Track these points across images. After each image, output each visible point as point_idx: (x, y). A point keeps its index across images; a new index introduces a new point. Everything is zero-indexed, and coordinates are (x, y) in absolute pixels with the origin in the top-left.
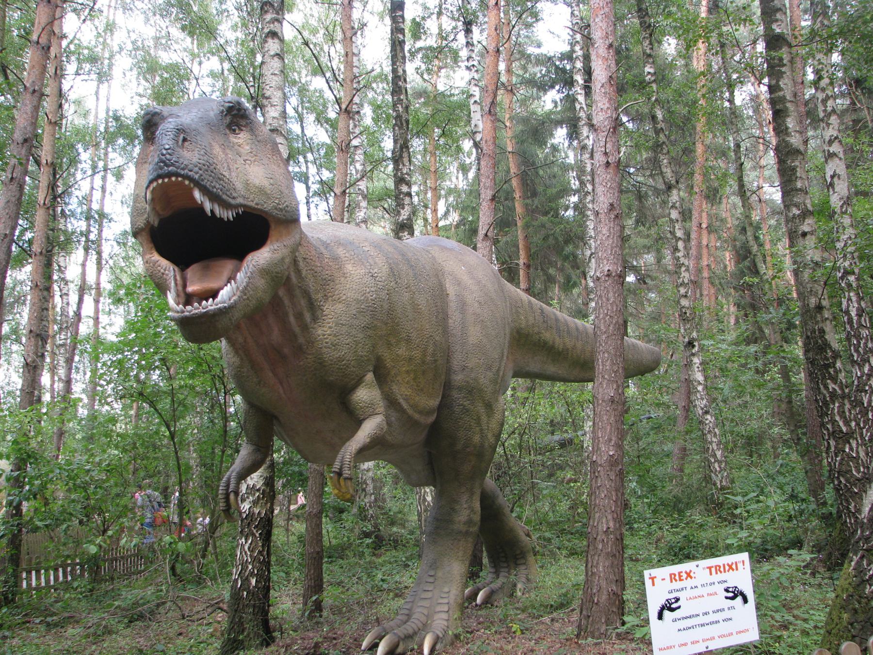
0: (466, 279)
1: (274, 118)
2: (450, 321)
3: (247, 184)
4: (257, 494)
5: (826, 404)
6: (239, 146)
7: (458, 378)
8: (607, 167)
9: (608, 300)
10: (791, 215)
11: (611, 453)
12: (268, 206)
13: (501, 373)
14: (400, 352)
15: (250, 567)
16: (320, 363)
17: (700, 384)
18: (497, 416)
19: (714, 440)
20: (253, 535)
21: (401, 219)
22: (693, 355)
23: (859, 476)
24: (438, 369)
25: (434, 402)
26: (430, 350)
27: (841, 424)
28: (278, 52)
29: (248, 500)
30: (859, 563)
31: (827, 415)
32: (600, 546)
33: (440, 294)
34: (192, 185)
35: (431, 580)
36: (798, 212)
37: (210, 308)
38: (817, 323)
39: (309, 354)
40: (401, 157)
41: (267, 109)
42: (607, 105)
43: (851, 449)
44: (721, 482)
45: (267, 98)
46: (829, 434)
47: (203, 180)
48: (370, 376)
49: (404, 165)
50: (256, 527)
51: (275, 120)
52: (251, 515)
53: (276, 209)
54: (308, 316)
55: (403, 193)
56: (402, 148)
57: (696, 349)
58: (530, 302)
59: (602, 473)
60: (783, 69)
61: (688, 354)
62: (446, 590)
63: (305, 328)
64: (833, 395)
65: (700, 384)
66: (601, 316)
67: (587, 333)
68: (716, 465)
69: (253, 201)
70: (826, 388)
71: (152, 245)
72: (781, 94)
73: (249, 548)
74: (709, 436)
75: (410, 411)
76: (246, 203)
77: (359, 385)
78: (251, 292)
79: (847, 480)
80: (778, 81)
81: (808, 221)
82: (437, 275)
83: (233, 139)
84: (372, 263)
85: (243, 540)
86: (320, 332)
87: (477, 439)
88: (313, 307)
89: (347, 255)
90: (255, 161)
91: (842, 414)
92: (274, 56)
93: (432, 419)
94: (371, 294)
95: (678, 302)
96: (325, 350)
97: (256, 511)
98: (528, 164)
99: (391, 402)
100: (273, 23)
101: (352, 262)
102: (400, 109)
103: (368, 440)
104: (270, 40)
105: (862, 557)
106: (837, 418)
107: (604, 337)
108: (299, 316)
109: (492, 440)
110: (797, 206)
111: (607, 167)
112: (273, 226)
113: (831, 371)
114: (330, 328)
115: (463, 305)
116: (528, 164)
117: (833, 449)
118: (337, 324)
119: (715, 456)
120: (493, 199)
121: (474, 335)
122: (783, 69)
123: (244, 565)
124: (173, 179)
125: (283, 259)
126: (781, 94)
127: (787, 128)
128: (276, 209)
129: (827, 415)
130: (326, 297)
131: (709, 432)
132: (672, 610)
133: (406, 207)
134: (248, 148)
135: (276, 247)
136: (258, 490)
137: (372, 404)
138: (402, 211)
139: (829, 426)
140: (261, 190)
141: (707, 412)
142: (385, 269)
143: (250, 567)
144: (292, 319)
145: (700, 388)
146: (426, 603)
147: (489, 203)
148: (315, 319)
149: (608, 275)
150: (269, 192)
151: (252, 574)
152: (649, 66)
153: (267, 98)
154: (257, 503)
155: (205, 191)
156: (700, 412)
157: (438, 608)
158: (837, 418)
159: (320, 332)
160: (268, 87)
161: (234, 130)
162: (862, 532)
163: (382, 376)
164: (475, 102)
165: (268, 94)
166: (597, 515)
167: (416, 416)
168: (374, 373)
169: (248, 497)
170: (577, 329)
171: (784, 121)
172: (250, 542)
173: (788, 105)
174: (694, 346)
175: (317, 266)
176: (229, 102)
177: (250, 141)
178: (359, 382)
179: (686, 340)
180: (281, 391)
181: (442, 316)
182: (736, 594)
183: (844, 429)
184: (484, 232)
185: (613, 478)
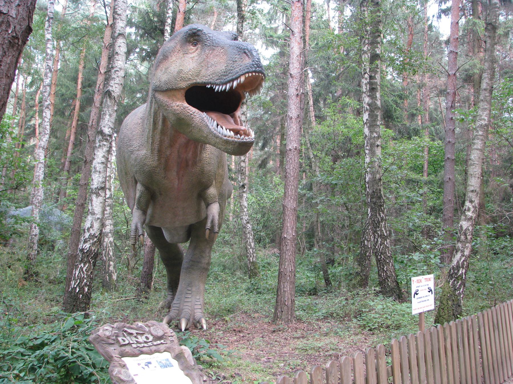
1: (122, 27)
4: (96, 239)
5: (379, 222)
9: (295, 161)
10: (373, 136)
15: (85, 281)
16: (202, 172)
17: (245, 207)
19: (251, 237)
22: (244, 192)
23: (389, 255)
27: (384, 232)
29: (89, 242)
30: (453, 283)
31: (379, 227)
32: (288, 278)
35: (189, 292)
36: (376, 136)
38: (378, 186)
41: (117, 21)
42: (298, 66)
43: (387, 243)
44: (253, 259)
45: (119, 15)
46: (378, 236)
50: (92, 257)
51: (122, 29)
57: (246, 189)
59: (289, 244)
60: (378, 70)
61: (241, 191)
62: (198, 297)
63: (201, 153)
64: (382, 219)
65: (245, 207)
68: (251, 250)
70: (380, 215)
71: (184, 98)
72: (376, 81)
73: (86, 270)
74: (248, 235)
79: (384, 257)
80: (375, 75)
81: (379, 140)
86: (205, 156)
91: (385, 227)
95: (240, 164)
97: (93, 249)
105: (454, 281)
106: (383, 229)
107: (292, 178)
110: (376, 133)
113: (382, 208)
117: (379, 242)
119: (250, 245)
122: (378, 70)
123: (81, 279)
126: (376, 81)
127: (376, 97)
129: (379, 227)
131: (249, 233)
132: (417, 294)
136: (96, 237)
137: (215, 197)
139: (379, 232)
141: (248, 223)
143: (85, 281)
145: (245, 210)
146: (189, 304)
149: (295, 149)
151: (86, 285)
153: (119, 15)
154: (94, 244)
156: (245, 222)
157: (196, 307)
158: (383, 229)
159: (205, 156)
160: (120, 9)
162: (453, 271)
165: (119, 12)
166: (287, 263)
169: (89, 241)
171: (376, 93)
172: (87, 266)
173: (378, 87)
174: (245, 188)
179: (241, 184)
182: (430, 291)
183: (385, 234)
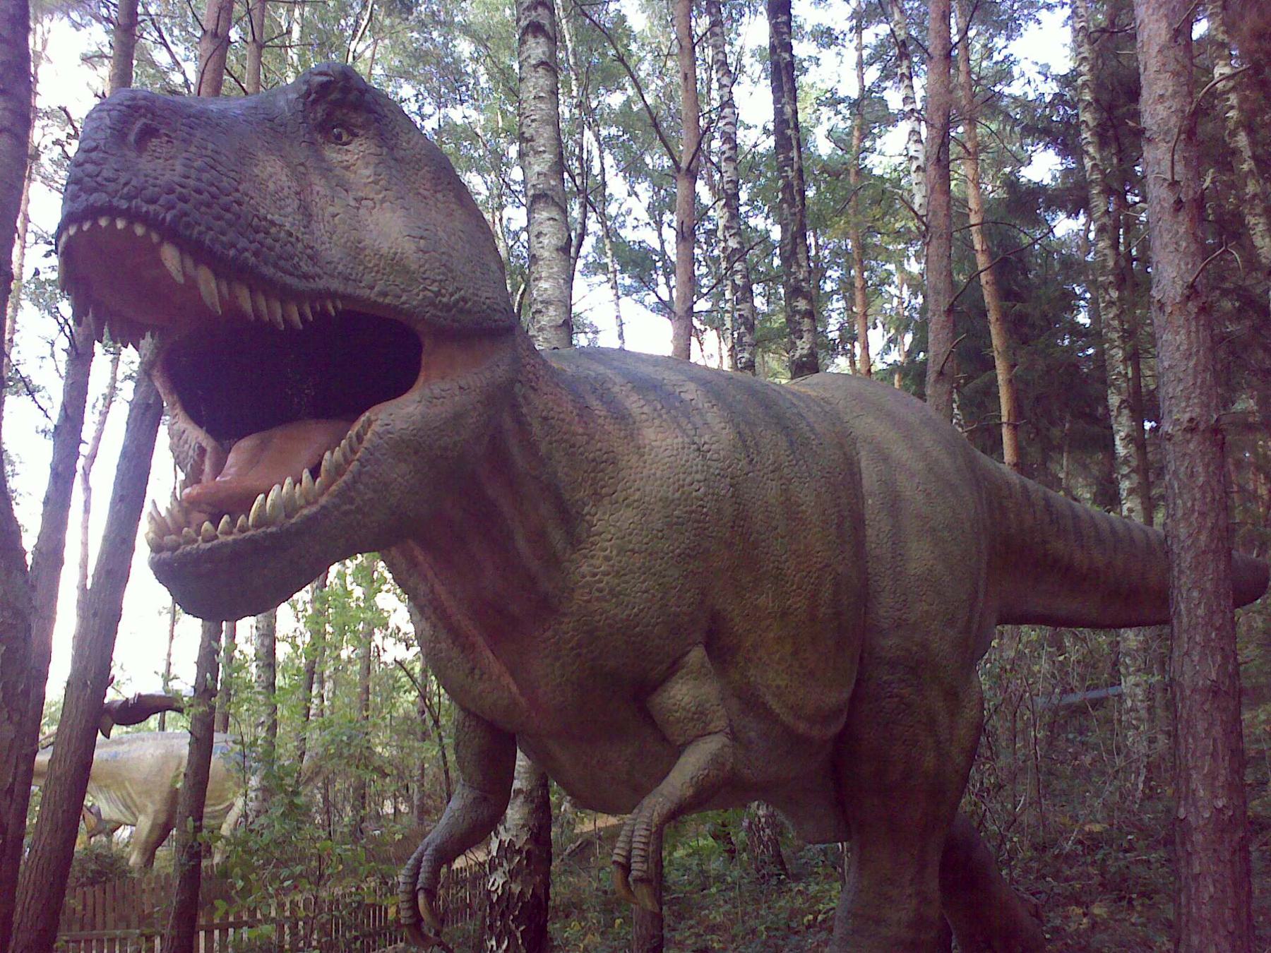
0: (900, 452)
2: (869, 532)
3: (356, 251)
6: (347, 168)
7: (890, 644)
8: (1177, 210)
11: (1220, 804)
12: (412, 299)
13: (975, 627)
14: (762, 601)
18: (970, 714)
20: (511, 935)
21: (797, 355)
24: (846, 621)
25: (836, 697)
26: (826, 593)
28: (544, 58)
29: (500, 870)
33: (848, 476)
34: (155, 237)
37: (222, 539)
39: (565, 615)
40: (794, 253)
47: (188, 225)
48: (697, 655)
49: (800, 266)
52: (506, 896)
53: (432, 304)
54: (557, 537)
55: (799, 312)
56: (794, 238)
58: (1024, 488)
63: (553, 562)
66: (1180, 513)
67: (1132, 540)
69: (373, 288)
75: (787, 718)
76: (350, 290)
77: (673, 674)
78: (370, 495)
82: (841, 446)
83: (333, 154)
84: (699, 423)
85: (494, 943)
86: (585, 569)
87: (929, 761)
88: (569, 517)
89: (646, 409)
90: (383, 201)
92: (538, 65)
93: (835, 728)
94: (696, 486)
96: (596, 605)
98: (1009, 263)
99: (750, 701)
100: (536, 9)
101: (657, 422)
102: (790, 173)
103: (690, 792)
104: (531, 41)
108: (538, 538)
109: (959, 759)
111: (1177, 210)
112: (427, 343)
114: (607, 559)
115: (894, 503)
116: (1009, 263)
118: (621, 551)
120: (950, 311)
121: (920, 556)
124: (103, 222)
125: (457, 417)
128: (432, 304)
130: (597, 497)
133: (806, 335)
134: (367, 172)
135: (437, 392)
136: (520, 851)
138: (798, 342)
140: (396, 264)
142: (726, 434)
144: (521, 543)
147: (943, 318)
148: (575, 542)
150: (414, 267)
152: (1222, 63)
155: (196, 251)
159: (585, 569)
161: (339, 137)
163: (721, 647)
164: (918, 167)
167: (802, 727)
168: (708, 647)
170: (1113, 531)
172: (504, 946)
175: (575, 434)
176: (321, 74)
177: (375, 160)
178: (674, 668)
180: (514, 689)
181: (852, 524)
184: (938, 368)
185: (1226, 855)
